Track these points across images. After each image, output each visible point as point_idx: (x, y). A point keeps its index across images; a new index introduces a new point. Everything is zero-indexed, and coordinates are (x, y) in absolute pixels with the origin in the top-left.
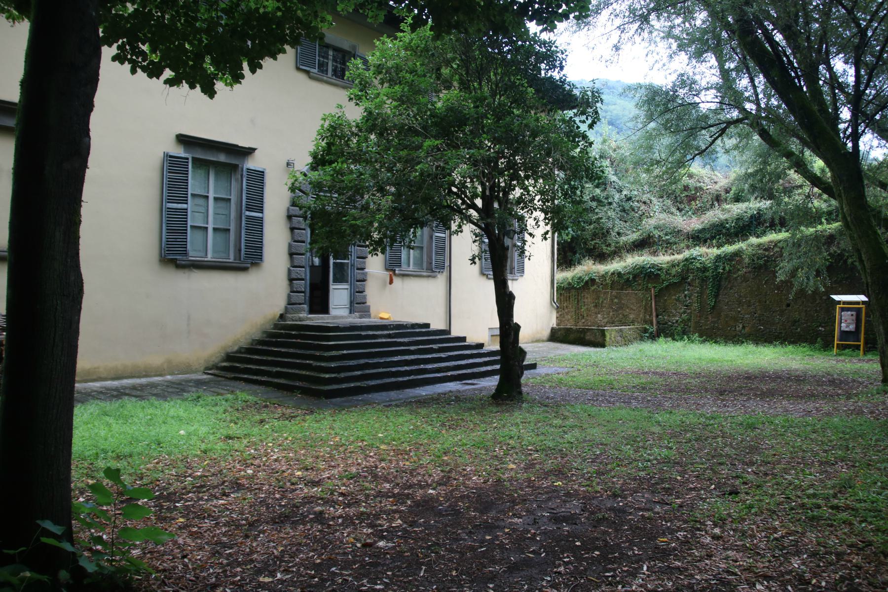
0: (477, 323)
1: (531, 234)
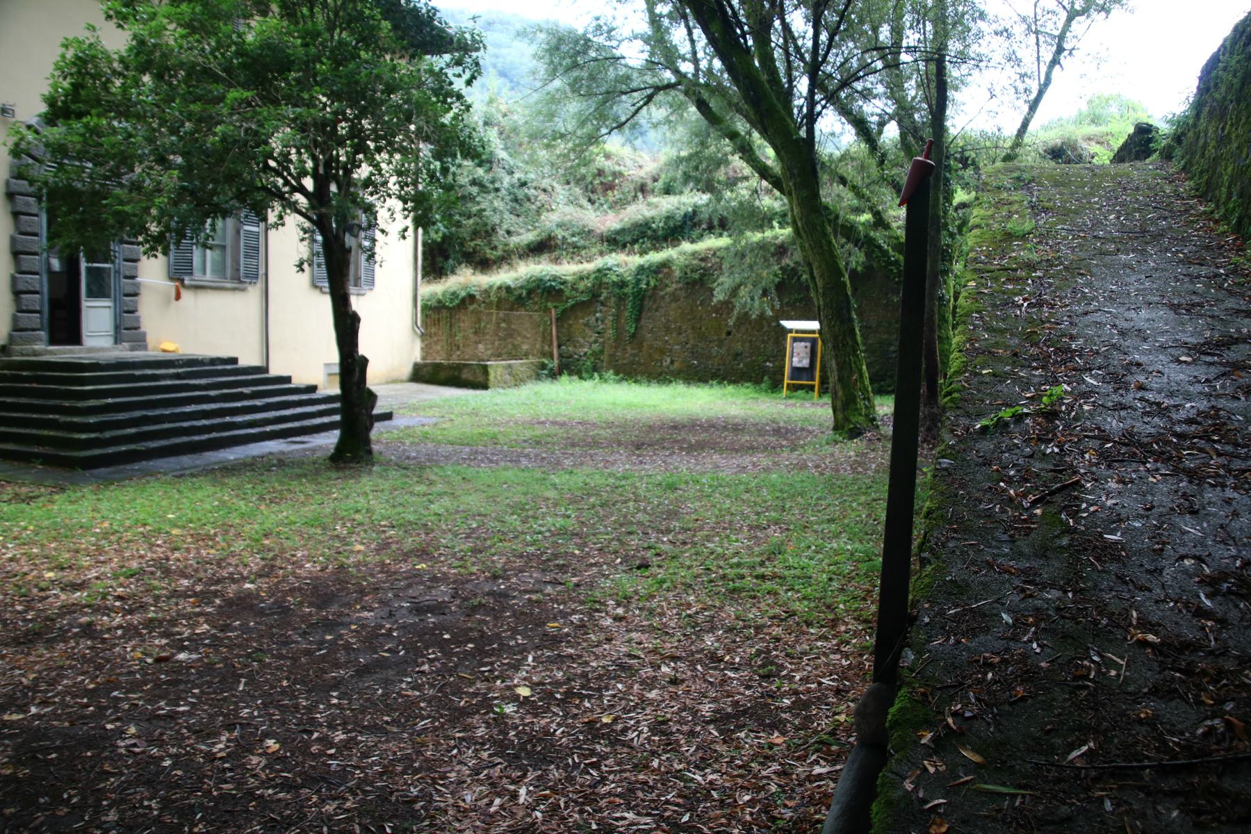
0: (309, 359)
1: (383, 231)
